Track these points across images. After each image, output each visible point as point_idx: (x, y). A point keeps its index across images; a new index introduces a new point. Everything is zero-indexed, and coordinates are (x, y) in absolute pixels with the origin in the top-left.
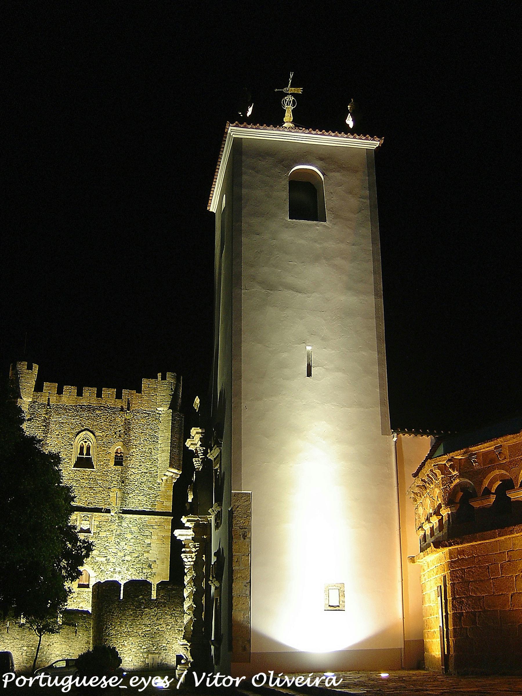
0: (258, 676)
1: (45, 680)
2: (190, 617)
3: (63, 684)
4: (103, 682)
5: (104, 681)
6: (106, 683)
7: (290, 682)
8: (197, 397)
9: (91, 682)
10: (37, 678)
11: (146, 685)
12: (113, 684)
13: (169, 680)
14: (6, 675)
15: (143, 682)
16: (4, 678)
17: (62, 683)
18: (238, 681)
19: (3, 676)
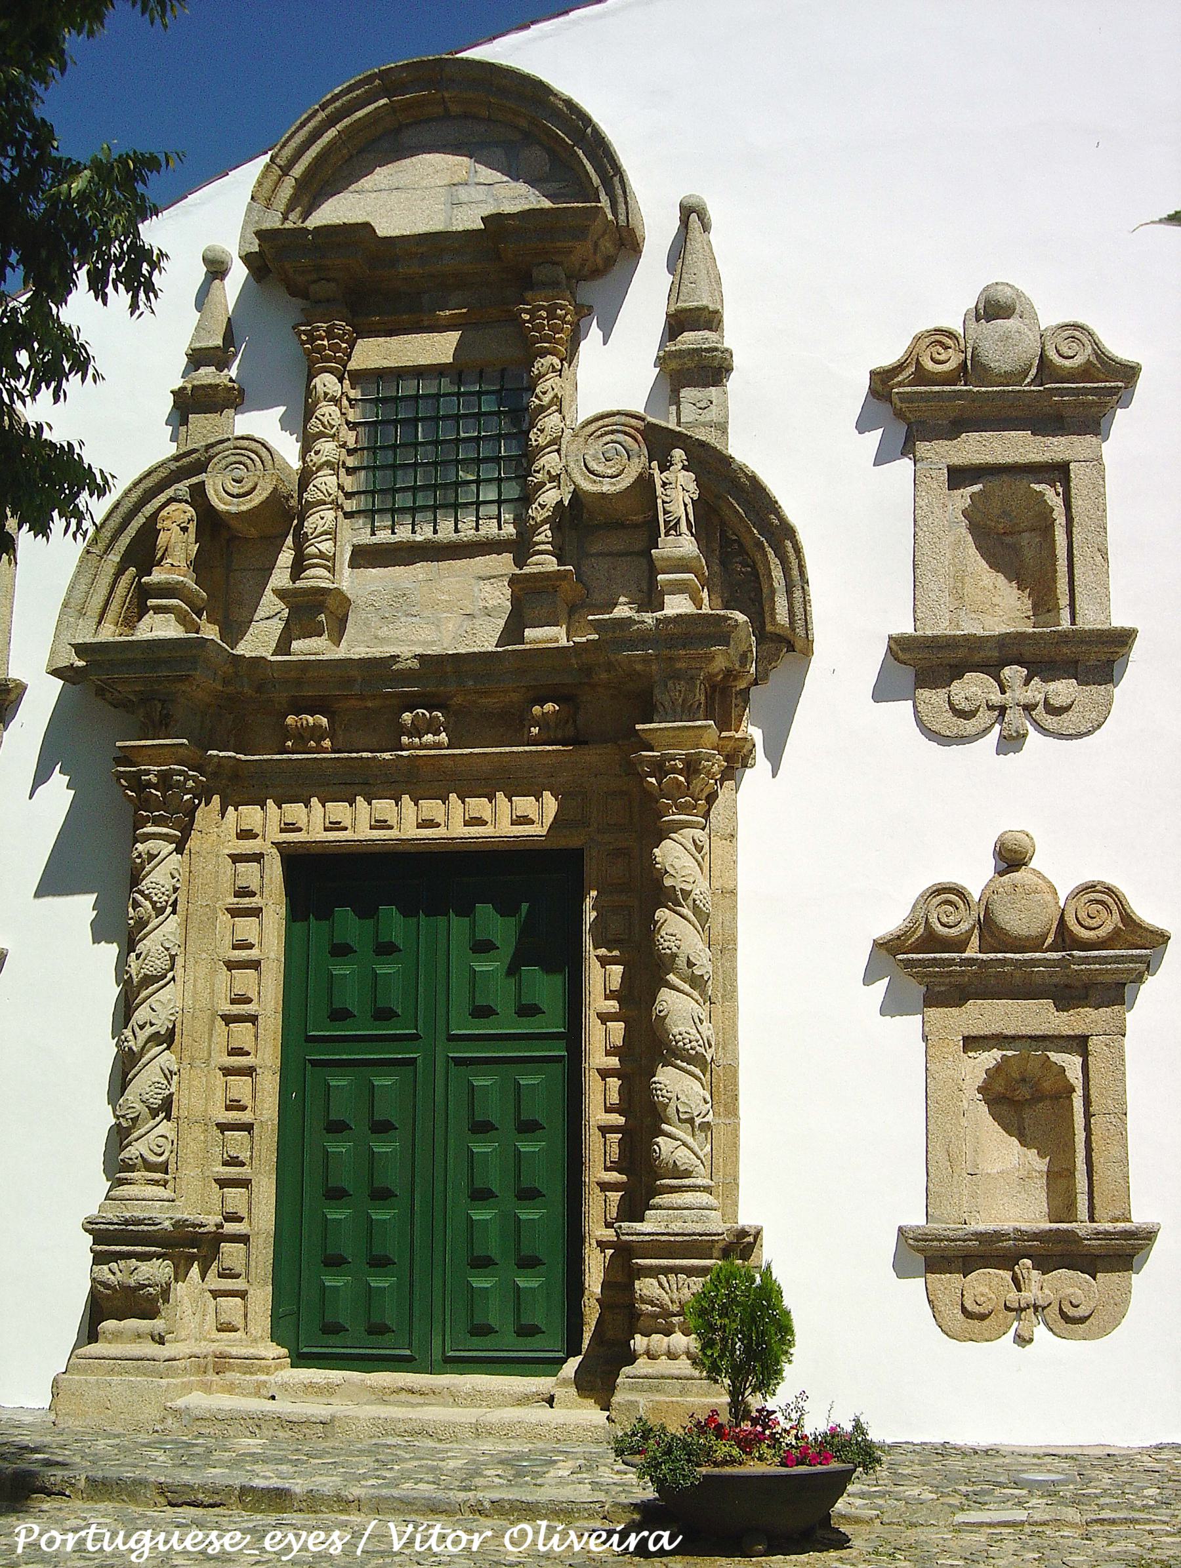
0: (515, 1530)
1: (98, 1538)
3: (134, 1547)
5: (337, 1541)
6: (217, 1545)
8: (887, 980)
10: (83, 1533)
11: (296, 1547)
12: (232, 1545)
16: (18, 1534)
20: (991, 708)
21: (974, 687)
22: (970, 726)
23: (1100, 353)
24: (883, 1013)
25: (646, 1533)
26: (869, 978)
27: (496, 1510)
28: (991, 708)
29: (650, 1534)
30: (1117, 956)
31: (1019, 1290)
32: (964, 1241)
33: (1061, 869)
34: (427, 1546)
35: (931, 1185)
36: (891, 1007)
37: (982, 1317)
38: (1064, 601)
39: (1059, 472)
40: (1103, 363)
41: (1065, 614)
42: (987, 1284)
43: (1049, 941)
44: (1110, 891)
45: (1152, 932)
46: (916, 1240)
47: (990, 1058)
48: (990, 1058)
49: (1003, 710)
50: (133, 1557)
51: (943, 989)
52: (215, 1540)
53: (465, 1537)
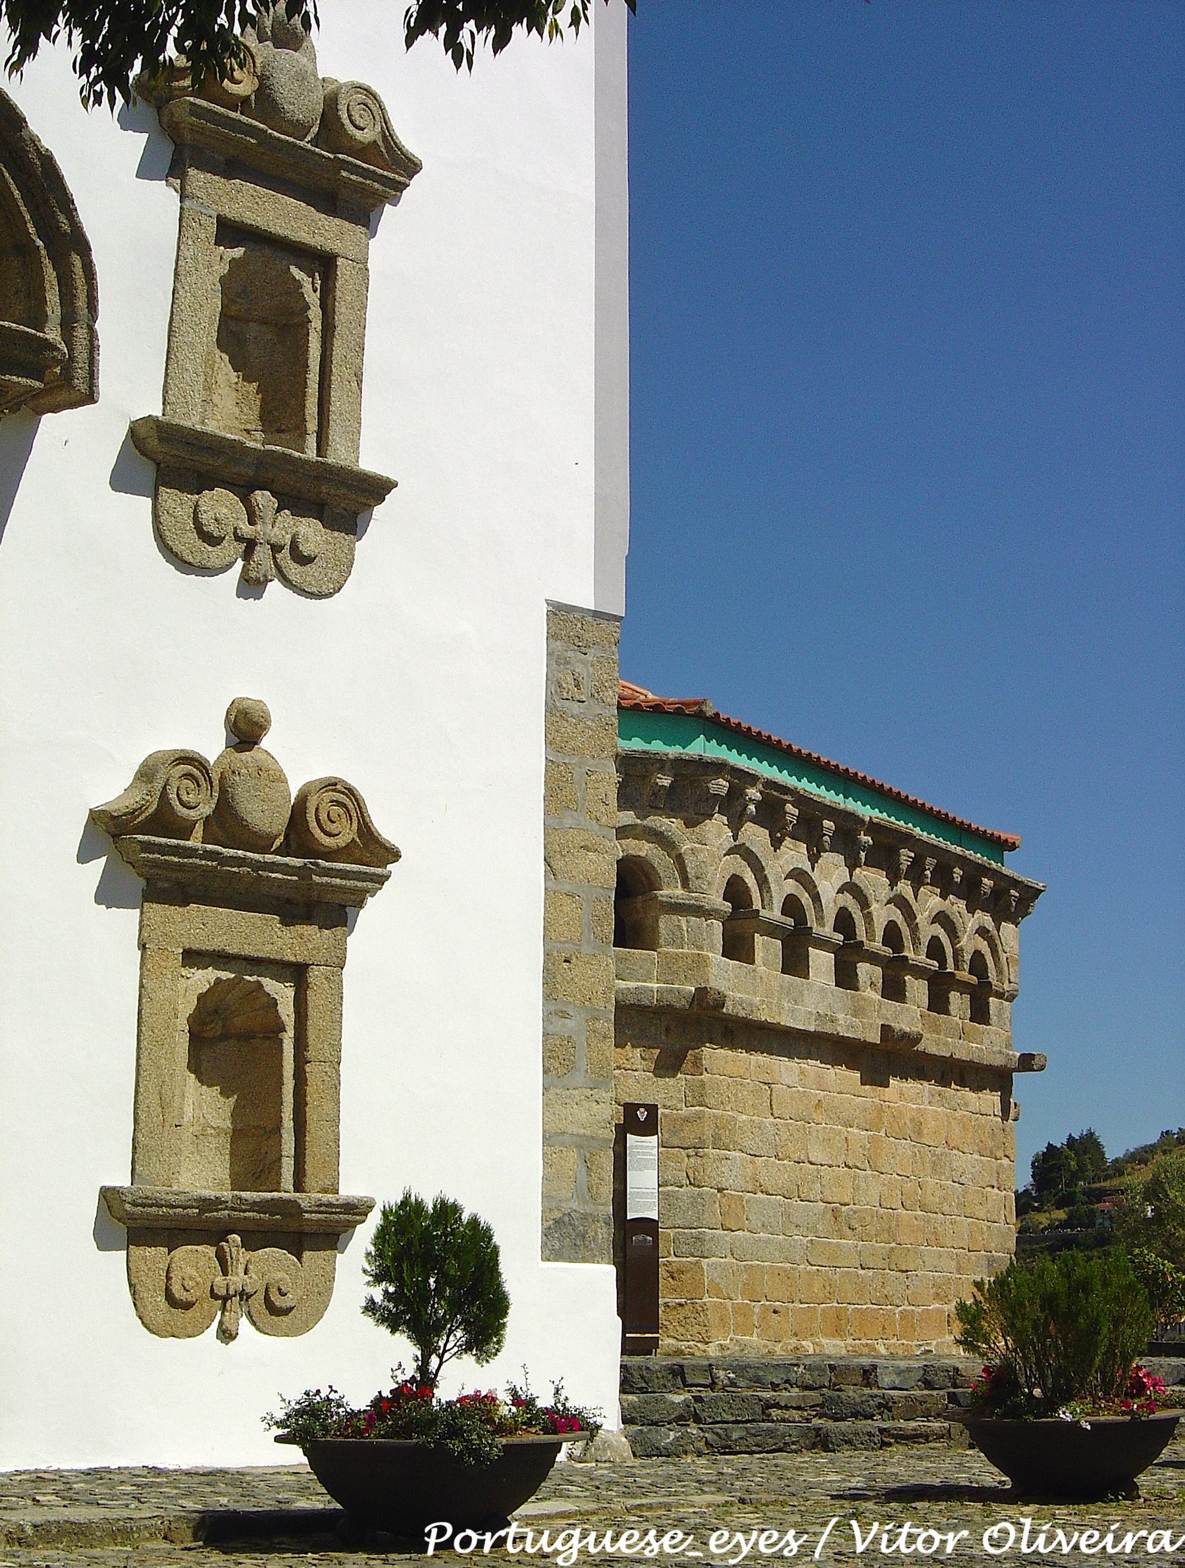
0: (996, 1528)
2: (959, 1356)
3: (561, 1548)
4: (787, 1544)
5: (792, 1541)
6: (655, 1546)
7: (747, 1541)
8: (105, 858)
9: (622, 1543)
10: (502, 1533)
11: (746, 1549)
13: (796, 1539)
14: (432, 1528)
15: (738, 1542)
16: (429, 1534)
17: (558, 1545)
18: (952, 1540)
19: (427, 1530)
20: (238, 538)
21: (220, 505)
22: (214, 555)
23: (388, 135)
24: (98, 900)
25: (1144, 1533)
26: (84, 856)
27: (41, 1538)
28: (238, 538)
29: (1150, 1534)
30: (374, 874)
31: (225, 1273)
32: (185, 1208)
33: (298, 757)
34: (894, 1547)
35: (139, 1135)
36: (107, 895)
37: (187, 1306)
38: (312, 426)
39: (323, 264)
40: (389, 148)
41: (311, 441)
42: (193, 1263)
43: (278, 843)
44: (350, 792)
45: (386, 848)
46: (134, 1204)
47: (203, 978)
48: (203, 978)
49: (250, 546)
50: (560, 1560)
51: (166, 885)
52: (653, 1541)
53: (937, 1537)
